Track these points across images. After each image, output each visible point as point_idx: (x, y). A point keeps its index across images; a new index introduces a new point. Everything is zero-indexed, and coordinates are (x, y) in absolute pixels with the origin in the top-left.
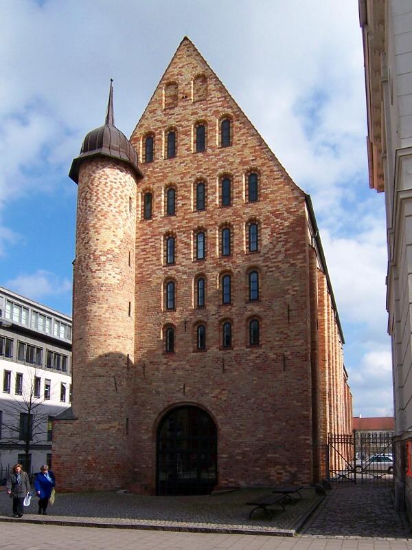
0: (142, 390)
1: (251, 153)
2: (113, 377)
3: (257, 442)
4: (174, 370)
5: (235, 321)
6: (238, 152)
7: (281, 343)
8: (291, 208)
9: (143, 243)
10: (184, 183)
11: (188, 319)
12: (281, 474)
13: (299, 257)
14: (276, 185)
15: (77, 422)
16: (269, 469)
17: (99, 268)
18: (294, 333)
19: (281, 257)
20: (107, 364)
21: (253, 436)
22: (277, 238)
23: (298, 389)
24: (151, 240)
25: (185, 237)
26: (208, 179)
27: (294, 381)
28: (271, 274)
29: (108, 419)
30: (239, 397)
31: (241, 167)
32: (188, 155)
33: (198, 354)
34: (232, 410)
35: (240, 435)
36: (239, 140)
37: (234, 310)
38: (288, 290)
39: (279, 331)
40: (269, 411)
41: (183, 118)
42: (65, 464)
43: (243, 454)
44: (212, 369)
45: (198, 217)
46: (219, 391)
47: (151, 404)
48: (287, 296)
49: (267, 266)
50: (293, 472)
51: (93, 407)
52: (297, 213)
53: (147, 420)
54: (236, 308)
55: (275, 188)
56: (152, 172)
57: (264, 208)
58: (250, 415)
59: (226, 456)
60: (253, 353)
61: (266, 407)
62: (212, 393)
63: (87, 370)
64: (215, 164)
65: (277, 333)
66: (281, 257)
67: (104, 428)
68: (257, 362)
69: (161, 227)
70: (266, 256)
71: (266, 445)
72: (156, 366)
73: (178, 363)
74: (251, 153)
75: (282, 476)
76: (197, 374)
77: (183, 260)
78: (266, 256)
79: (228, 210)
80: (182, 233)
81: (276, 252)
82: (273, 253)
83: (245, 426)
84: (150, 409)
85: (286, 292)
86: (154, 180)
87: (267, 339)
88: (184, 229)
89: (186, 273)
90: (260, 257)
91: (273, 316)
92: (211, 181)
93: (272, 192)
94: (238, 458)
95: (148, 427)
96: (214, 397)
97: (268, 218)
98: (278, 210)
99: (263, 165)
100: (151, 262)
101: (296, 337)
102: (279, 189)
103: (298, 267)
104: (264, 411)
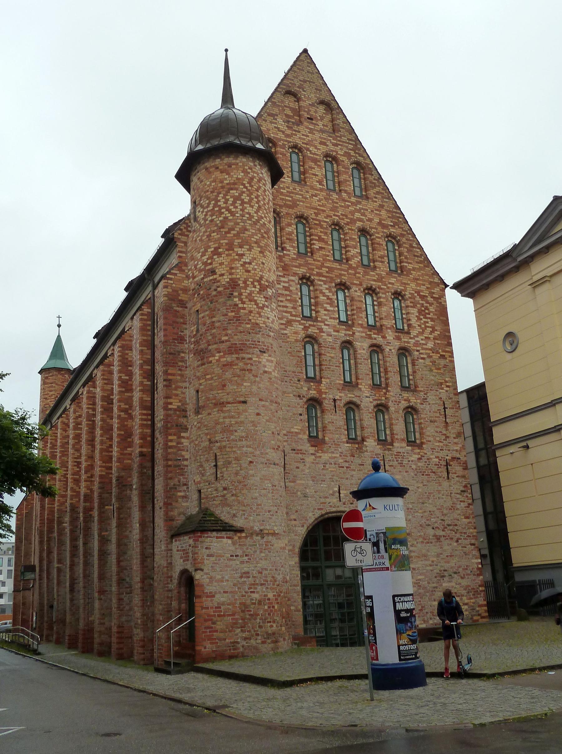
1: (389, 217)
5: (392, 409)
7: (441, 444)
8: (434, 293)
10: (319, 221)
17: (266, 303)
25: (327, 289)
36: (376, 198)
47: (297, 511)
51: (269, 511)
52: (440, 301)
55: (417, 266)
64: (352, 213)
72: (300, 456)
77: (325, 317)
78: (416, 339)
80: (322, 283)
84: (295, 520)
86: (281, 203)
89: (331, 336)
90: (411, 338)
93: (414, 269)
95: (294, 546)
98: (422, 291)
99: (402, 235)
100: (285, 309)
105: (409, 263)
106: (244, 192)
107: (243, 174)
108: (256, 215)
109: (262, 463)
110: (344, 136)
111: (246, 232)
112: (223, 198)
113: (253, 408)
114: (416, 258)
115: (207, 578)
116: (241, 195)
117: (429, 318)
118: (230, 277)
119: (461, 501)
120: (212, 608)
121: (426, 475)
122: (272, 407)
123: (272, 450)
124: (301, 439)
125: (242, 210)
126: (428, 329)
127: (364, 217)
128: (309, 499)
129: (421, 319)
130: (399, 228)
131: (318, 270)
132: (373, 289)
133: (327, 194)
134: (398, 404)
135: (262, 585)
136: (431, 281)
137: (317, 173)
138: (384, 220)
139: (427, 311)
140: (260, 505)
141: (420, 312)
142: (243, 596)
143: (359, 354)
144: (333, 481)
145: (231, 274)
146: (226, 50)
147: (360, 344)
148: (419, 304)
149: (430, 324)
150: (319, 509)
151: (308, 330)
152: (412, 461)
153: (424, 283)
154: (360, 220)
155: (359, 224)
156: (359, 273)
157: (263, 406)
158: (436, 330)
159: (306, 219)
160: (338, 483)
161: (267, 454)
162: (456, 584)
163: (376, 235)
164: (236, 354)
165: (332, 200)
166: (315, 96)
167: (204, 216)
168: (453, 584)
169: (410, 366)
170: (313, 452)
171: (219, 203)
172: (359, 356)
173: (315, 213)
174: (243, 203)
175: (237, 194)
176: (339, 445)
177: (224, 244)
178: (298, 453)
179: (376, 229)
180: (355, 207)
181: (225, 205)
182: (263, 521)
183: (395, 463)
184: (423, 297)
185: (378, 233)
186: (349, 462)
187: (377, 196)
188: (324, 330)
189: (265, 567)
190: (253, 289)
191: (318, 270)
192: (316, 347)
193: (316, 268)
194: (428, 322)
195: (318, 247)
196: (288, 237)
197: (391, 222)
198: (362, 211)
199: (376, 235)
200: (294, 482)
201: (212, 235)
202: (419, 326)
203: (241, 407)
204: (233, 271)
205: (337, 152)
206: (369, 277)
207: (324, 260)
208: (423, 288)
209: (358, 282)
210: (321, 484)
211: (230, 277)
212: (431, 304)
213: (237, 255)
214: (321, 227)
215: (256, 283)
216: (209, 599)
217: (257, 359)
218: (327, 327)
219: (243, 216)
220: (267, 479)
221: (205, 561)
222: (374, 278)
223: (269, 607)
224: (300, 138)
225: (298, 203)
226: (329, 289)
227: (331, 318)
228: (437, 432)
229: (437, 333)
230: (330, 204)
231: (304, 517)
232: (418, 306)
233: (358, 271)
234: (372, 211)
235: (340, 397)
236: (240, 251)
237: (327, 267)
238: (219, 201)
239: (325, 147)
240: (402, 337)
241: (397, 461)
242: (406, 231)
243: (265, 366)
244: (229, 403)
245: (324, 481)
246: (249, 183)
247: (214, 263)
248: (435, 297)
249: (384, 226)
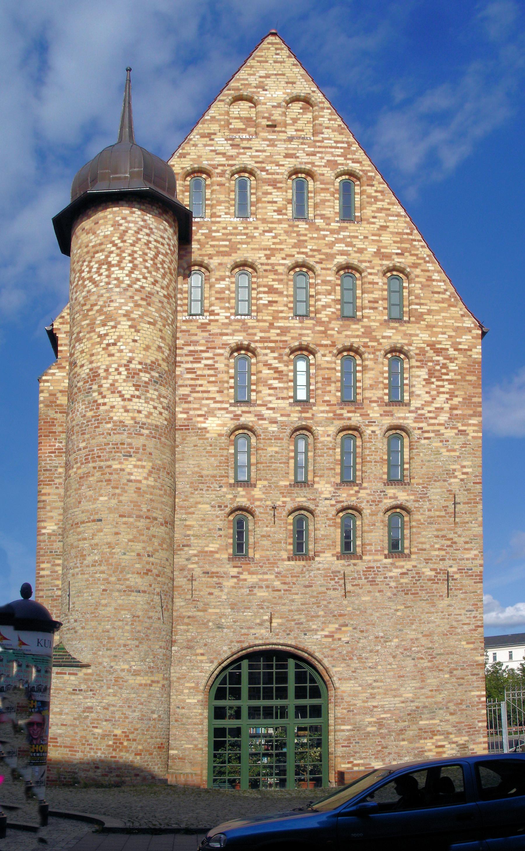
0: (186, 620)
1: (395, 242)
2: (158, 594)
3: (403, 705)
4: (252, 588)
5: (366, 512)
6: (373, 235)
7: (443, 553)
8: (460, 343)
9: (191, 359)
10: (272, 265)
11: (279, 503)
12: (443, 746)
13: (471, 422)
14: (437, 302)
15: (89, 671)
16: (422, 741)
17: (137, 393)
18: (463, 539)
19: (443, 418)
20: (150, 571)
21: (395, 696)
22: (437, 386)
23: (469, 624)
24: (205, 355)
25: (275, 358)
26: (318, 267)
27: (463, 612)
28: (426, 441)
29: (149, 668)
30: (371, 637)
31: (376, 261)
32: (280, 221)
33: (298, 563)
34: (360, 658)
35: (373, 696)
36: (374, 217)
37: (363, 494)
38: (454, 470)
39: (441, 533)
40: (422, 658)
41: (270, 159)
42: (59, 740)
43: (380, 724)
44: (324, 589)
45: (301, 328)
46: (337, 626)
47: (205, 645)
48: (452, 480)
49: (421, 428)
50: (461, 742)
51: (125, 646)
52: (469, 353)
53: (196, 672)
54: (368, 491)
55: (435, 307)
56: (208, 236)
57: (417, 335)
58: (390, 664)
59: (349, 727)
60: (397, 567)
61: (418, 652)
62: (323, 630)
63: (113, 579)
64: (331, 245)
65: (437, 537)
66: (443, 418)
67: (144, 682)
68: (402, 581)
69: (227, 334)
70: (420, 412)
71: (418, 707)
72: (215, 579)
73: (260, 577)
74: (395, 242)
75: (444, 749)
76: (296, 597)
78: (420, 412)
79: (354, 326)
80: (268, 351)
81: (436, 408)
82: (430, 409)
83: (382, 681)
84: (202, 654)
85: (451, 474)
86: (211, 251)
87: (420, 546)
88: (272, 345)
89: (276, 423)
90: (410, 412)
91: (430, 510)
92: (324, 272)
93: (429, 312)
94: (369, 729)
95: (197, 684)
96: (326, 636)
97: (422, 352)
98: (440, 343)
99: (415, 266)
100: (205, 395)
101: (467, 546)
102: (442, 310)
103: (469, 437)
104: (413, 659)
105: (420, 304)
106: (111, 252)
107: (112, 229)
108: (127, 278)
109: (119, 591)
111: (112, 304)
113: (110, 526)
114: (436, 295)
117: (447, 380)
118: (90, 366)
121: (412, 594)
122: (139, 524)
123: (136, 576)
124: (218, 559)
126: (441, 395)
127: (350, 249)
128: (225, 630)
129: (433, 383)
130: (412, 255)
131: (262, 335)
133: (290, 226)
134: (376, 505)
136: (458, 327)
137: (275, 200)
138: (386, 247)
140: (113, 638)
141: (431, 373)
143: (321, 442)
144: (262, 608)
145: (91, 362)
147: (323, 429)
148: (432, 361)
149: (448, 387)
150: (238, 642)
151: (239, 419)
152: (391, 577)
153: (445, 330)
154: (342, 253)
155: (341, 260)
156: (333, 329)
157: (125, 523)
158: (457, 396)
159: (252, 266)
160: (269, 611)
161: (128, 580)
163: (369, 271)
164: (93, 462)
169: (406, 450)
170: (235, 574)
172: (319, 445)
173: (266, 255)
174: (110, 265)
176: (276, 563)
178: (212, 577)
179: (370, 262)
180: (336, 236)
183: (363, 581)
185: (373, 268)
186: (289, 583)
187: (377, 214)
190: (117, 377)
191: (262, 335)
192: (253, 440)
193: (261, 331)
195: (266, 302)
196: (218, 296)
197: (398, 248)
198: (349, 240)
199: (369, 271)
200: (205, 610)
203: (95, 526)
204: (94, 358)
206: (349, 333)
207: (274, 318)
208: (441, 337)
209: (329, 342)
210: (243, 612)
212: (452, 360)
214: (276, 272)
215: (122, 369)
217: (118, 466)
218: (271, 412)
220: (125, 610)
222: (357, 333)
225: (239, 246)
226: (279, 359)
227: (278, 399)
230: (293, 238)
231: (215, 651)
233: (331, 326)
234: (366, 237)
235: (284, 502)
236: (102, 331)
237: (279, 328)
241: (366, 578)
243: (130, 474)
244: (83, 522)
245: (249, 608)
246: (121, 238)
248: (461, 349)
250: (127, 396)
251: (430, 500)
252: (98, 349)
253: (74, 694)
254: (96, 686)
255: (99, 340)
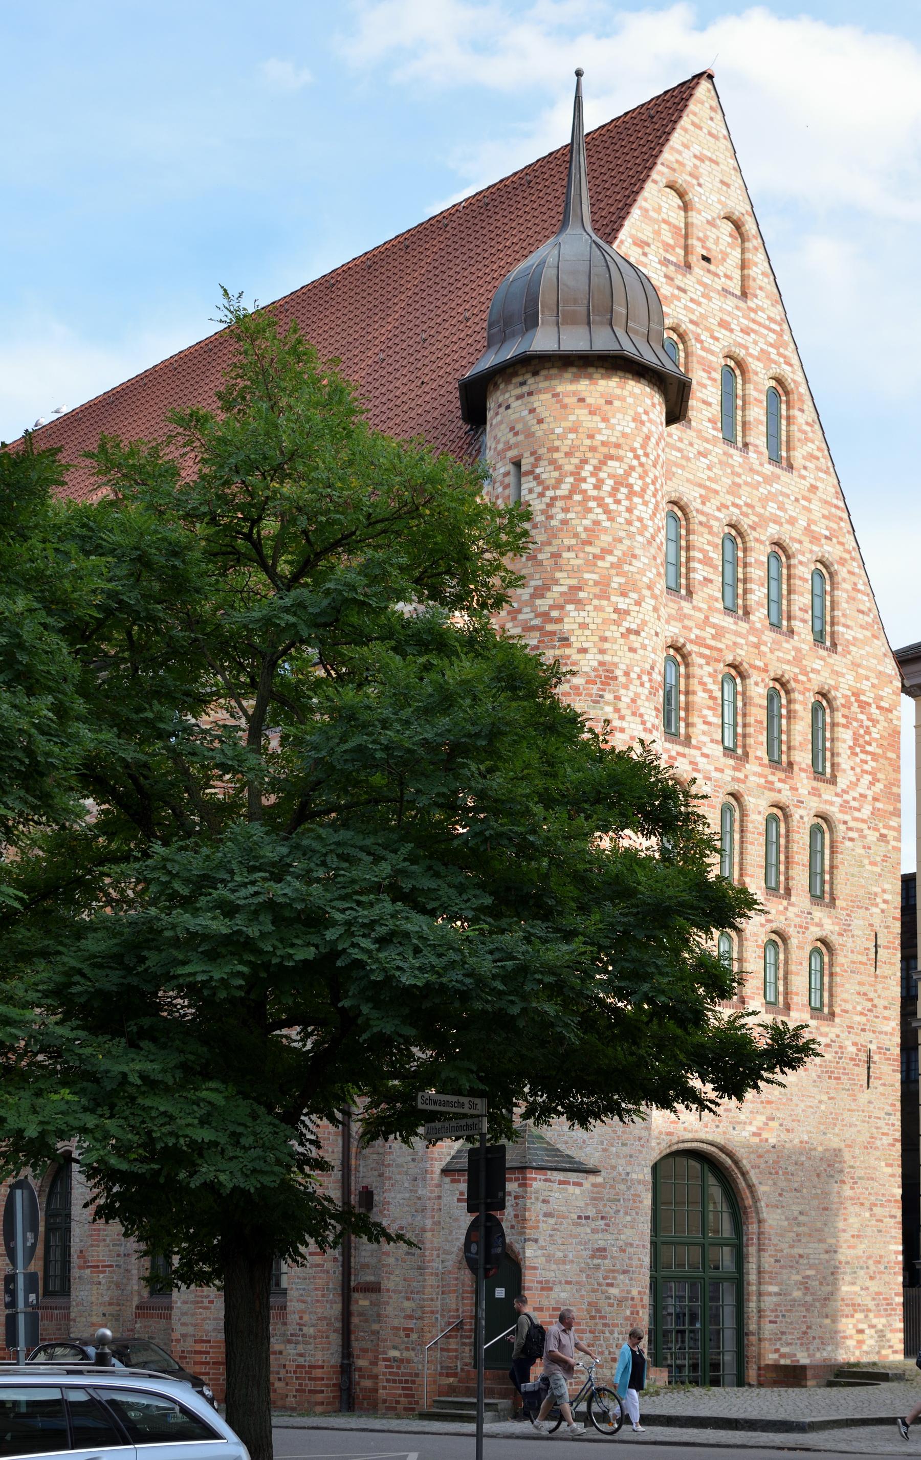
15: (599, 1179)
66: (866, 812)
78: (846, 797)
99: (842, 561)
105: (847, 626)
106: (632, 468)
110: (763, 310)
111: (634, 562)
112: (592, 474)
115: (543, 1255)
116: (628, 474)
118: (600, 657)
119: (883, 1134)
120: (548, 1309)
125: (629, 510)
129: (857, 755)
132: (784, 680)
135: (625, 1272)
136: (880, 672)
139: (867, 738)
142: (594, 1291)
143: (752, 822)
146: (579, 74)
148: (856, 720)
153: (869, 674)
162: (862, 1289)
165: (732, 466)
166: (719, 201)
167: (544, 507)
168: (857, 1288)
171: (584, 486)
175: (621, 472)
177: (591, 583)
179: (801, 542)
180: (768, 487)
181: (595, 493)
182: (631, 1156)
184: (863, 705)
188: (700, 766)
189: (630, 1241)
190: (640, 690)
194: (866, 762)
197: (827, 528)
198: (781, 498)
201: (565, 555)
202: (853, 769)
204: (607, 645)
205: (747, 348)
206: (781, 654)
207: (710, 608)
211: (600, 657)
213: (616, 611)
216: (545, 1293)
218: (704, 760)
219: (629, 523)
221: (541, 1225)
223: (632, 1313)
224: (686, 308)
228: (859, 994)
229: (879, 786)
232: (855, 724)
234: (797, 500)
236: (623, 603)
237: (714, 626)
238: (584, 480)
239: (727, 333)
240: (822, 791)
242: (850, 552)
247: (566, 620)
249: (815, 539)
250: (649, 725)
251: (853, 936)
252: (613, 632)
253: (580, 1225)
254: (609, 1210)
255: (615, 616)
